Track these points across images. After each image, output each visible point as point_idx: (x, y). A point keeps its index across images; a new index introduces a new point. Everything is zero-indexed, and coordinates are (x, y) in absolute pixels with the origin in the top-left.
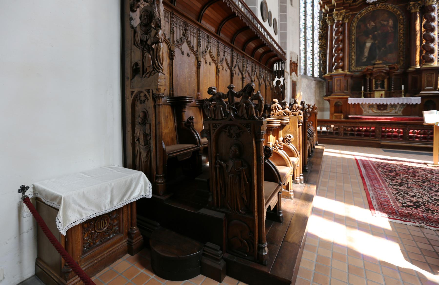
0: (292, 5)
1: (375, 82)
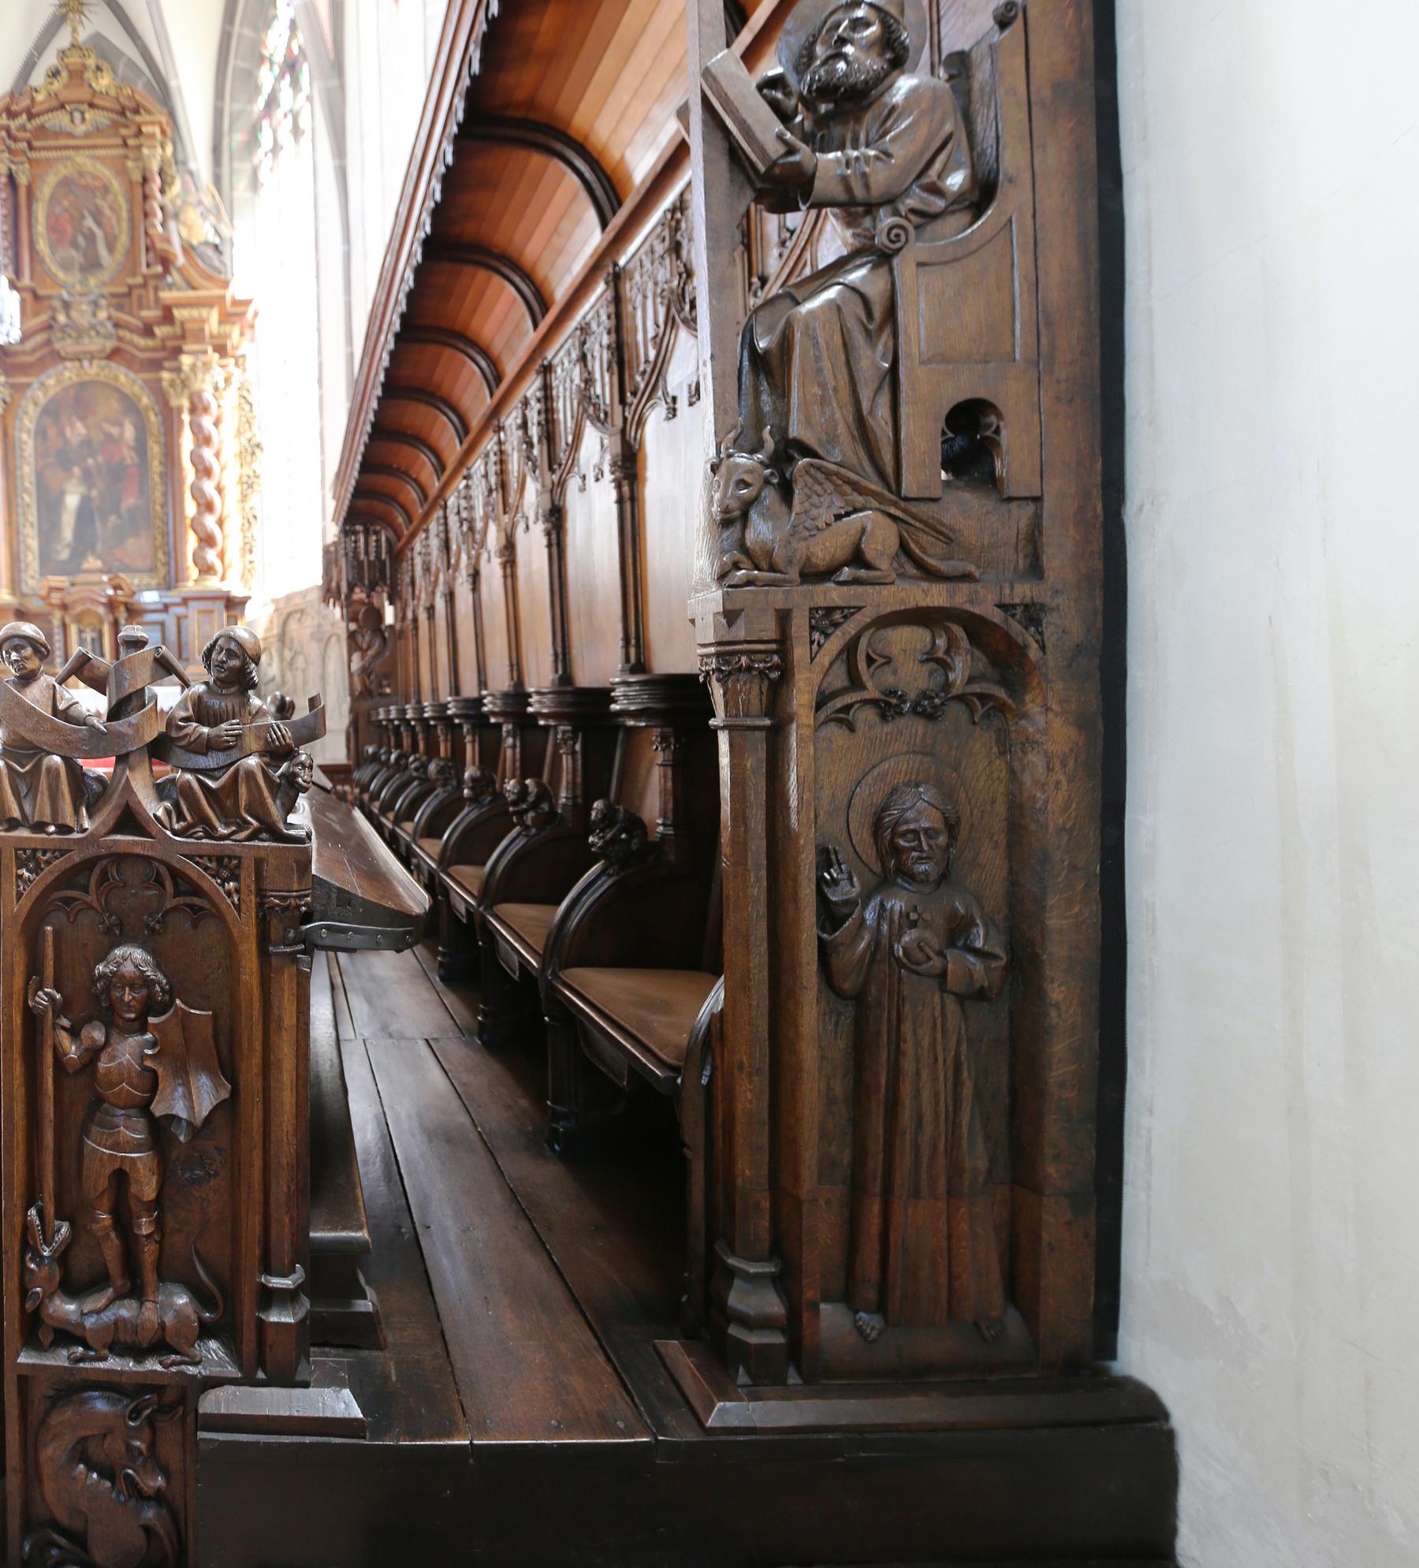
1: (80, 632)
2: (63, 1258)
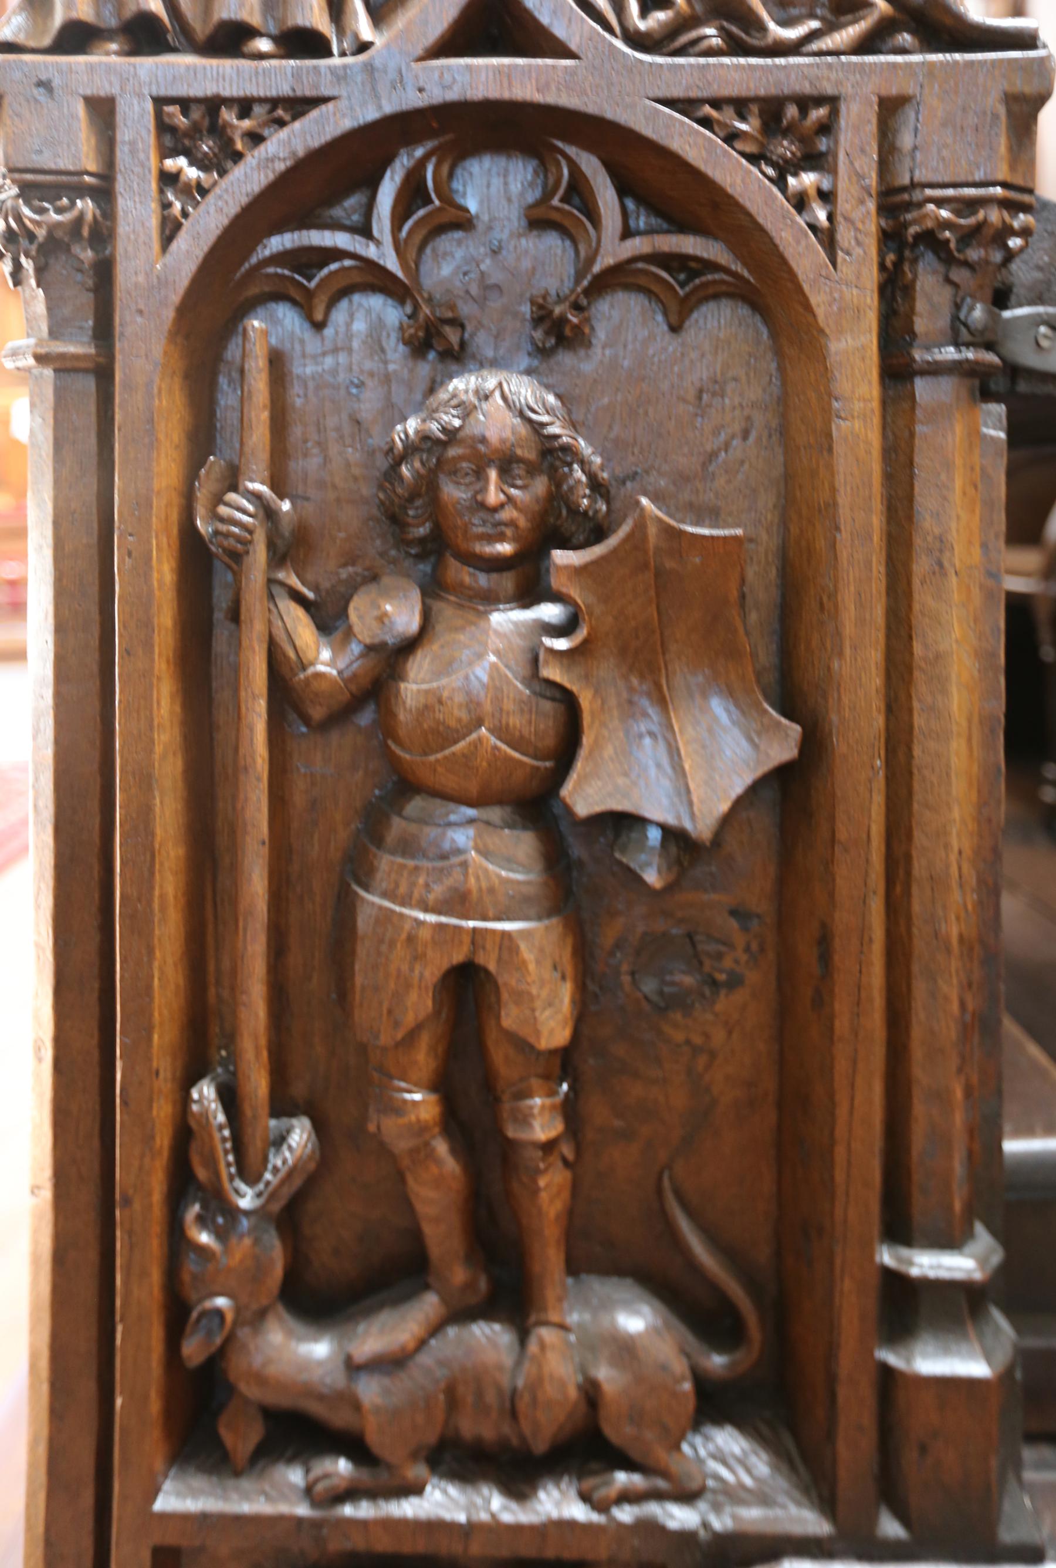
2: (289, 1215)
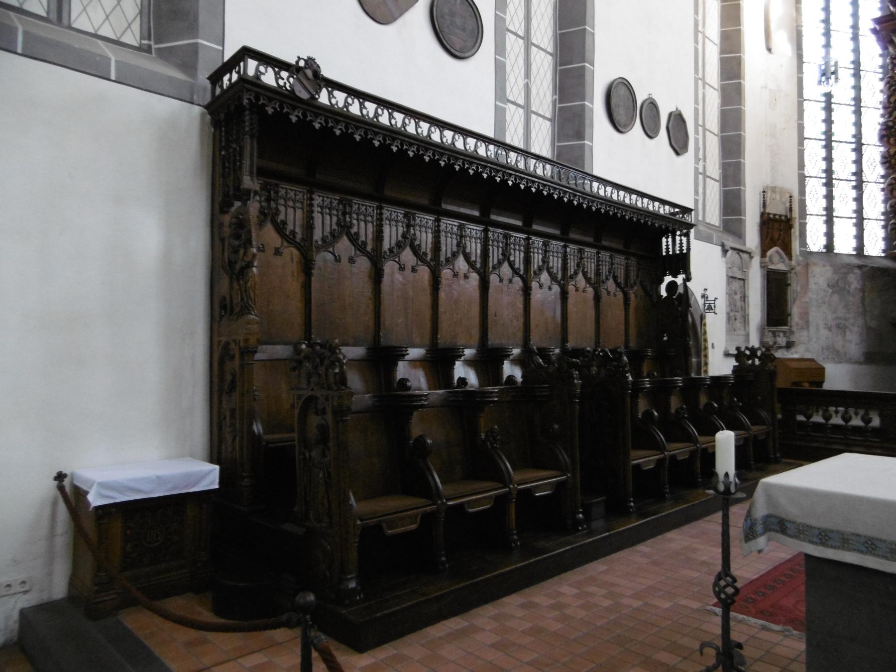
0: (769, 50)
